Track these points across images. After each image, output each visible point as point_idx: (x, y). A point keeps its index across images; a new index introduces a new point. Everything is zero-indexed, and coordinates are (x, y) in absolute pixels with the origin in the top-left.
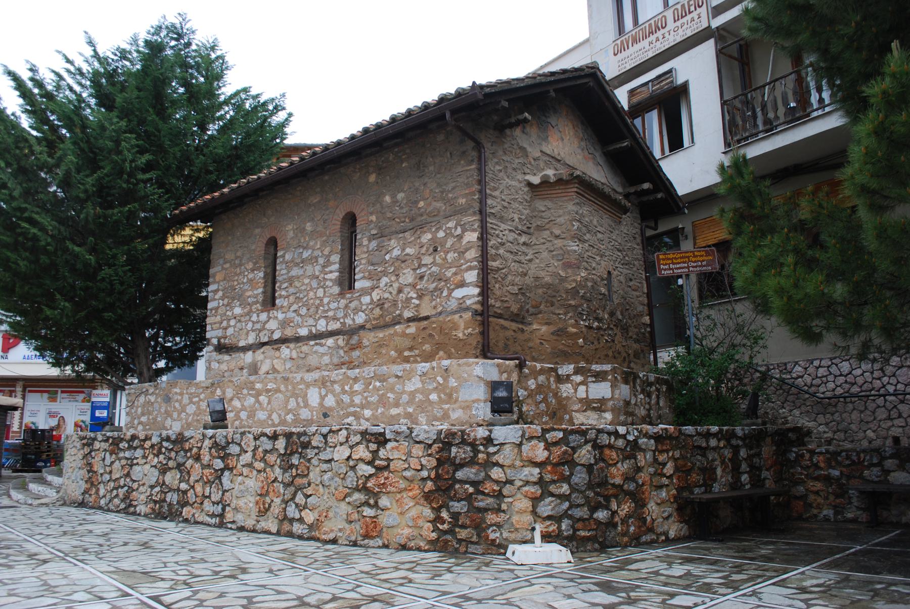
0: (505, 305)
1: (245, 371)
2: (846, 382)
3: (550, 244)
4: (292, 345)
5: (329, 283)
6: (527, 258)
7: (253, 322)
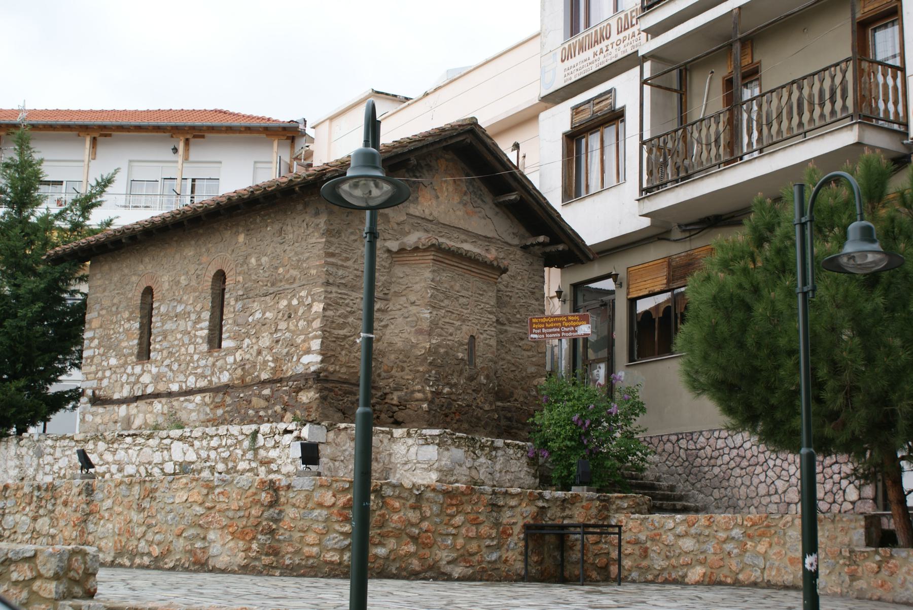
0: (352, 371)
1: (119, 424)
2: (738, 455)
3: (406, 310)
4: (164, 400)
5: (199, 340)
6: (383, 323)
7: (128, 375)
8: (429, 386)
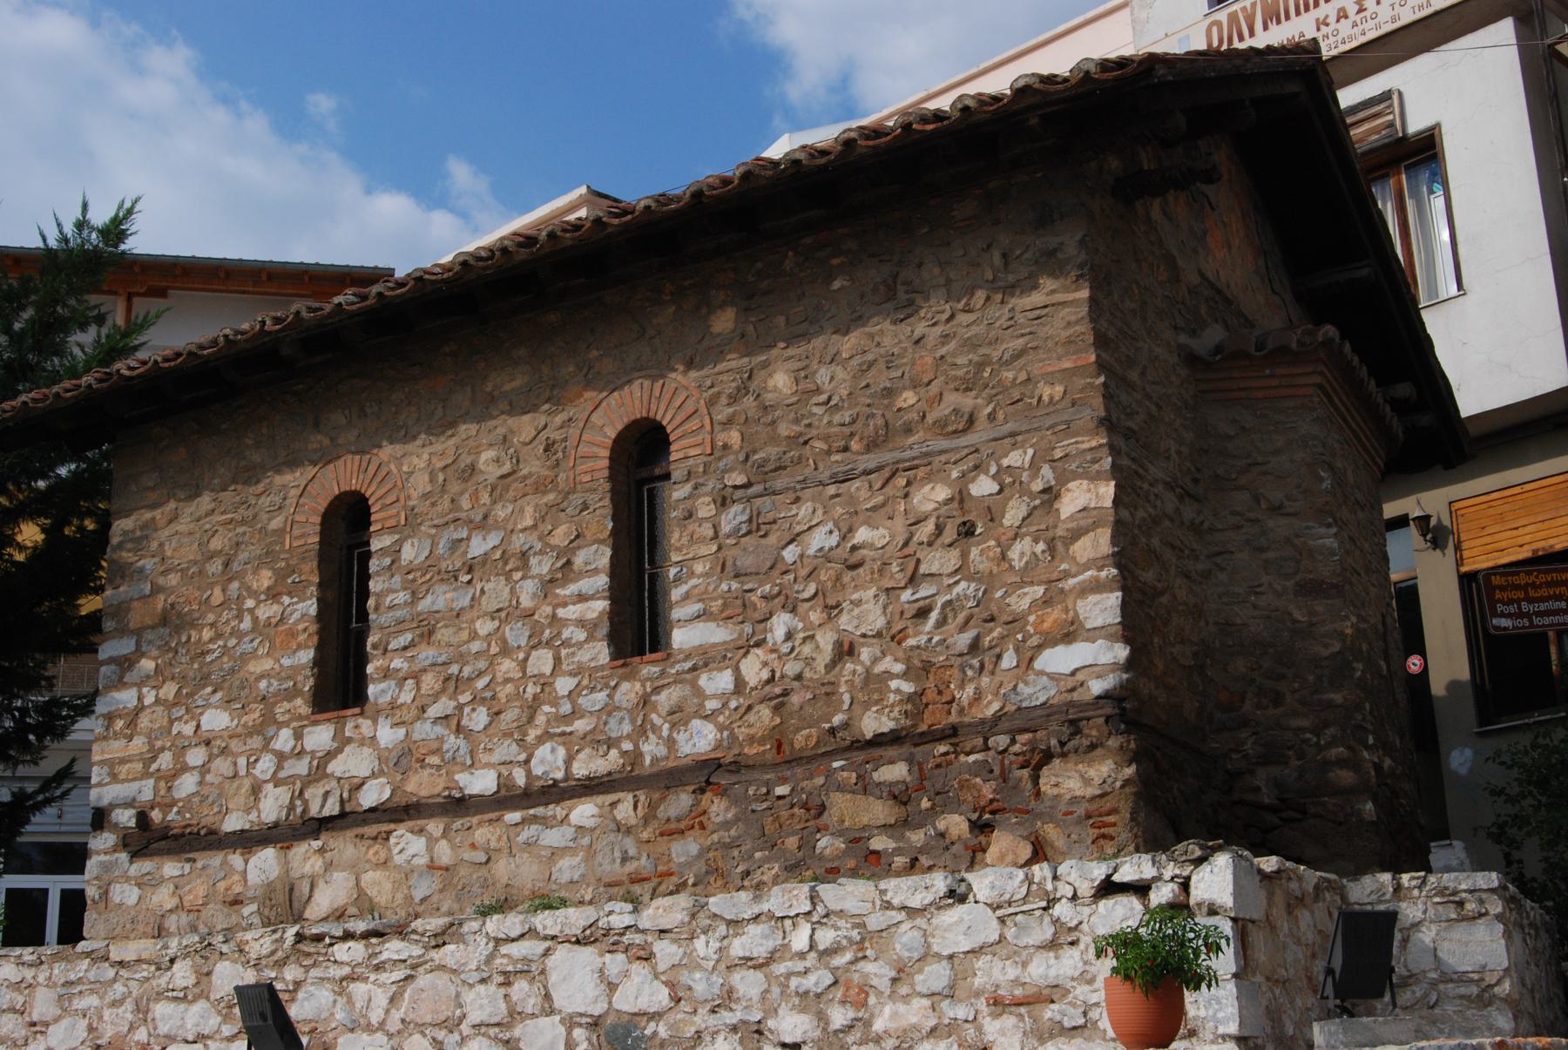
4: (435, 826)
7: (281, 757)
8: (1367, 747)
